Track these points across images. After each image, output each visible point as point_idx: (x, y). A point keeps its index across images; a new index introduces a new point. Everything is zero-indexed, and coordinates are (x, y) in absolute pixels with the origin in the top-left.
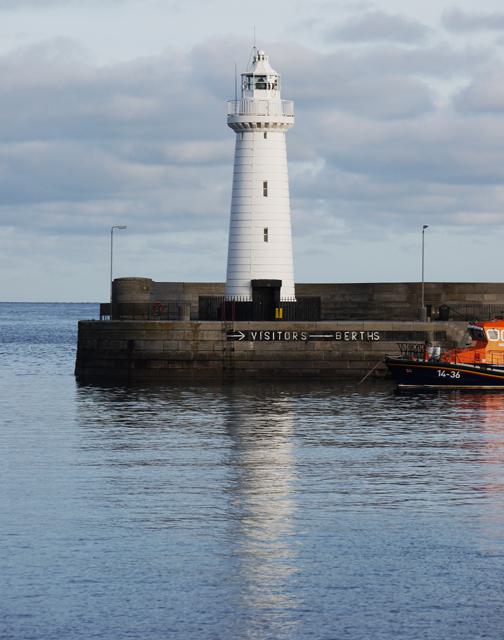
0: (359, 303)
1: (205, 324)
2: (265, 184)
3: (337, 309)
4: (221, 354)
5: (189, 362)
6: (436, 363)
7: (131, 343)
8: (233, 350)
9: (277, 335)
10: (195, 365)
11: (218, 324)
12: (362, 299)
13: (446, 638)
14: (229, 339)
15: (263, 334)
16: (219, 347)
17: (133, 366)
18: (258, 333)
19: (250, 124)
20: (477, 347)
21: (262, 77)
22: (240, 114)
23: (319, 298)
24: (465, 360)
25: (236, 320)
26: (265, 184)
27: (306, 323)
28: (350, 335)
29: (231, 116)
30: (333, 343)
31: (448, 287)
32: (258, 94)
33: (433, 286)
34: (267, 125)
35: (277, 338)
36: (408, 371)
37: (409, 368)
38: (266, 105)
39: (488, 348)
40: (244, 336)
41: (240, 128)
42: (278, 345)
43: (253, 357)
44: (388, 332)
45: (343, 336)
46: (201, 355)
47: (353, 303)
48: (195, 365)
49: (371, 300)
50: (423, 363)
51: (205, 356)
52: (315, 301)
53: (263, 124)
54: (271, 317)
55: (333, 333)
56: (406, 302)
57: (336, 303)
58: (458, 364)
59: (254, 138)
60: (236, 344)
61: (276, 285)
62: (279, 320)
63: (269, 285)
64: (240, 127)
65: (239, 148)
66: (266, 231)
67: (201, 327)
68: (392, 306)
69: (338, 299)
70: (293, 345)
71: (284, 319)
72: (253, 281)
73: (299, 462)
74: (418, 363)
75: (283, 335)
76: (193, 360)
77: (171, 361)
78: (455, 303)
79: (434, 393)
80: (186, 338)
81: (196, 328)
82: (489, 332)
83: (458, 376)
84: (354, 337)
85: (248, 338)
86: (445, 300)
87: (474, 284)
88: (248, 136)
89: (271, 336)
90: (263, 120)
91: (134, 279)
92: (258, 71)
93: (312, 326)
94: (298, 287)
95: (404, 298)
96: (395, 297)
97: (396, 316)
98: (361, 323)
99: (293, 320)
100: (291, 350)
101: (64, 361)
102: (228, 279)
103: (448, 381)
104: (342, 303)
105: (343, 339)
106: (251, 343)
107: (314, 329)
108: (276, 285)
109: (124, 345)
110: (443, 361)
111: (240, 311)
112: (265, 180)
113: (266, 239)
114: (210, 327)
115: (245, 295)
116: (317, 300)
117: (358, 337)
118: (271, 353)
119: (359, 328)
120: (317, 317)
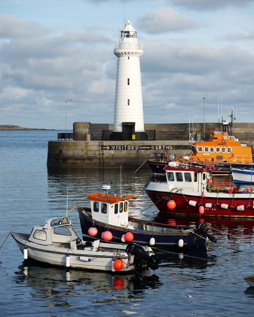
0: (180, 132)
2: (129, 80)
4: (98, 156)
5: (84, 160)
7: (61, 151)
8: (103, 154)
9: (124, 147)
10: (87, 161)
11: (97, 143)
13: (59, 315)
14: (102, 149)
16: (97, 153)
17: (61, 161)
18: (116, 146)
21: (128, 32)
28: (158, 147)
30: (150, 151)
32: (126, 39)
33: (212, 124)
34: (129, 53)
35: (124, 149)
36: (158, 167)
37: (158, 165)
41: (118, 55)
42: (125, 152)
43: (113, 158)
44: (176, 146)
45: (155, 148)
48: (87, 161)
51: (91, 157)
53: (127, 53)
54: (131, 139)
55: (150, 146)
59: (124, 59)
60: (105, 151)
61: (132, 125)
63: (129, 125)
64: (120, 54)
67: (89, 144)
69: (173, 130)
70: (131, 152)
72: (123, 123)
77: (76, 159)
81: (87, 146)
84: (160, 148)
85: (111, 148)
88: (121, 58)
91: (81, 123)
92: (126, 30)
93: (140, 143)
94: (145, 125)
98: (163, 141)
99: (140, 140)
101: (42, 155)
102: (115, 122)
104: (174, 132)
105: (155, 149)
106: (112, 151)
107: (141, 145)
108: (132, 125)
109: (58, 153)
111: (115, 136)
114: (93, 144)
115: (119, 129)
117: (162, 148)
118: (121, 156)
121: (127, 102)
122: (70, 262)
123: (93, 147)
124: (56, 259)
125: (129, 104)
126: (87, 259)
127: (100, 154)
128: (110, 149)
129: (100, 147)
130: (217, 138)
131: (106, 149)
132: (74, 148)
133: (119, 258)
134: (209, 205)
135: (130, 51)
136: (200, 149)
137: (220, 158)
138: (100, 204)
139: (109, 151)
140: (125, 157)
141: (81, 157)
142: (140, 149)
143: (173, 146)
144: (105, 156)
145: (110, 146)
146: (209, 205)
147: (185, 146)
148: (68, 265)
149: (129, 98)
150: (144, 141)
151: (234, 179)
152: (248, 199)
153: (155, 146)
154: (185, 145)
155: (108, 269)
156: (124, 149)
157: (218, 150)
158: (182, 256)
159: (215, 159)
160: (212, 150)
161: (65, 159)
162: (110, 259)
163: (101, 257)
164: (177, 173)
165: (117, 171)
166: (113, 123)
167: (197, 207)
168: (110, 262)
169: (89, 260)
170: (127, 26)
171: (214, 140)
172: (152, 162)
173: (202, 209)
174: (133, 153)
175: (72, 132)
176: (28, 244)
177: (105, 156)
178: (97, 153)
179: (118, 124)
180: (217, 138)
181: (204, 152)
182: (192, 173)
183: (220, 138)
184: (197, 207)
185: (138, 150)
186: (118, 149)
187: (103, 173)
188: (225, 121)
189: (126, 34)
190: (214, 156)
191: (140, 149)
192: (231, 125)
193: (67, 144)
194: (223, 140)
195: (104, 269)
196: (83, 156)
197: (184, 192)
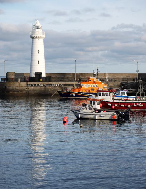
0: (62, 78)
1: (22, 83)
2: (38, 51)
3: (57, 79)
4: (25, 89)
5: (18, 91)
6: (69, 92)
7: (6, 87)
8: (28, 88)
9: (39, 85)
10: (20, 92)
11: (25, 83)
12: (63, 77)
14: (27, 86)
16: (25, 88)
17: (6, 92)
19: (37, 37)
20: (80, 88)
23: (51, 77)
24: (76, 91)
25: (29, 82)
26: (38, 51)
27: (45, 82)
28: (56, 85)
29: (31, 35)
30: (52, 87)
31: (82, 74)
34: (38, 37)
35: (39, 86)
36: (63, 94)
38: (39, 33)
39: (82, 89)
41: (33, 38)
42: (39, 87)
43: (33, 90)
45: (54, 85)
47: (61, 78)
48: (20, 92)
49: (65, 77)
50: (66, 92)
51: (22, 90)
52: (49, 78)
54: (39, 81)
55: (52, 85)
56: (72, 77)
57: (57, 78)
59: (36, 40)
60: (29, 87)
61: (40, 74)
65: (33, 41)
66: (38, 61)
67: (21, 83)
68: (70, 78)
69: (58, 77)
70: (41, 87)
71: (42, 81)
72: (35, 73)
73: (48, 117)
74: (65, 92)
77: (14, 91)
78: (84, 77)
79: (69, 100)
81: (20, 84)
82: (82, 84)
83: (74, 95)
86: (81, 77)
87: (88, 73)
90: (37, 36)
91: (11, 72)
95: (72, 76)
96: (69, 76)
97: (70, 80)
98: (58, 82)
102: (30, 72)
103: (72, 96)
104: (58, 78)
105: (54, 86)
107: (47, 84)
108: (40, 74)
109: (4, 88)
110: (71, 91)
111: (31, 79)
115: (33, 76)
116: (51, 77)
117: (58, 85)
119: (57, 83)
120: (50, 81)
121: (38, 62)
122: (97, 117)
123: (23, 84)
124: (92, 117)
125: (38, 63)
126: (103, 116)
127: (26, 89)
128: (31, 86)
130: (91, 80)
131: (29, 86)
132: (13, 86)
133: (114, 115)
134: (116, 105)
135: (39, 36)
138: (92, 102)
140: (39, 90)
142: (47, 86)
143: (63, 85)
144: (29, 89)
145: (31, 85)
146: (116, 105)
147: (69, 84)
148: (96, 118)
150: (48, 82)
152: (132, 103)
153: (54, 84)
154: (69, 84)
155: (110, 119)
156: (39, 86)
158: (120, 118)
159: (90, 90)
161: (8, 91)
162: (110, 116)
163: (108, 115)
164: (102, 93)
165: (55, 96)
166: (29, 73)
167: (112, 106)
168: (111, 116)
169: (104, 116)
170: (37, 23)
171: (90, 81)
172: (60, 92)
173: (113, 107)
174: (43, 88)
175: (6, 77)
176: (80, 113)
177: (29, 89)
178: (25, 88)
179: (33, 73)
180: (91, 80)
181: (85, 87)
182: (109, 93)
184: (112, 106)
187: (28, 98)
188: (95, 72)
189: (36, 27)
190: (90, 89)
191: (47, 86)
192: (97, 74)
193: (9, 83)
195: (109, 119)
196: (18, 89)
197: (106, 100)
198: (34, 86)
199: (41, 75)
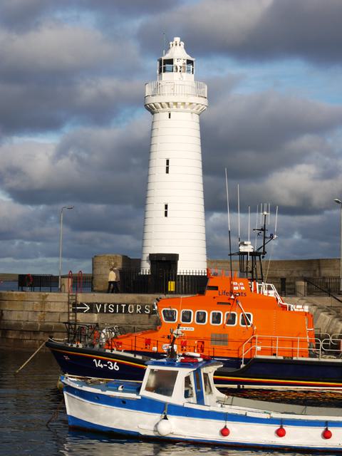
5: (36, 332)
9: (121, 308)
14: (75, 311)
15: (107, 307)
16: (65, 319)
18: (103, 305)
19: (168, 104)
22: (153, 96)
26: (168, 161)
34: (176, 104)
35: (120, 311)
40: (89, 308)
46: (48, 326)
58: (115, 352)
59: (162, 116)
61: (171, 260)
62: (171, 293)
63: (164, 259)
67: (48, 299)
70: (136, 318)
74: (77, 350)
75: (126, 308)
76: (40, 331)
77: (22, 332)
80: (35, 309)
81: (43, 303)
83: (115, 367)
85: (92, 310)
89: (115, 308)
99: (138, 293)
100: (134, 323)
106: (96, 315)
108: (171, 260)
112: (167, 157)
113: (166, 215)
128: (91, 311)
129: (71, 306)
130: (216, 288)
131: (82, 311)
136: (170, 316)
137: (223, 339)
139: (89, 315)
141: (31, 326)
145: (91, 305)
149: (166, 202)
151: (68, 413)
156: (120, 311)
157: (217, 318)
159: (207, 344)
160: (201, 318)
171: (208, 293)
180: (216, 288)
183: (223, 287)
185: (149, 314)
186: (108, 312)
194: (232, 292)
198: (102, 311)
199: (175, 264)
